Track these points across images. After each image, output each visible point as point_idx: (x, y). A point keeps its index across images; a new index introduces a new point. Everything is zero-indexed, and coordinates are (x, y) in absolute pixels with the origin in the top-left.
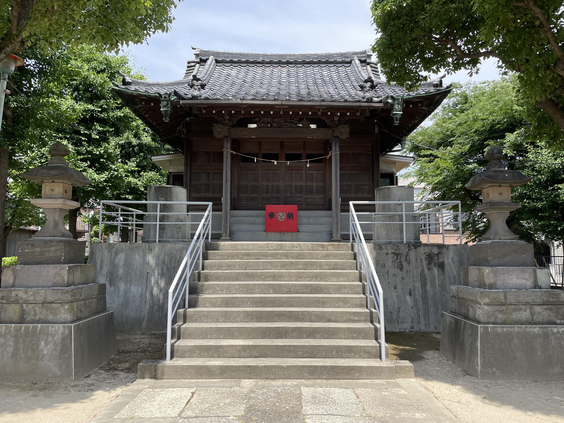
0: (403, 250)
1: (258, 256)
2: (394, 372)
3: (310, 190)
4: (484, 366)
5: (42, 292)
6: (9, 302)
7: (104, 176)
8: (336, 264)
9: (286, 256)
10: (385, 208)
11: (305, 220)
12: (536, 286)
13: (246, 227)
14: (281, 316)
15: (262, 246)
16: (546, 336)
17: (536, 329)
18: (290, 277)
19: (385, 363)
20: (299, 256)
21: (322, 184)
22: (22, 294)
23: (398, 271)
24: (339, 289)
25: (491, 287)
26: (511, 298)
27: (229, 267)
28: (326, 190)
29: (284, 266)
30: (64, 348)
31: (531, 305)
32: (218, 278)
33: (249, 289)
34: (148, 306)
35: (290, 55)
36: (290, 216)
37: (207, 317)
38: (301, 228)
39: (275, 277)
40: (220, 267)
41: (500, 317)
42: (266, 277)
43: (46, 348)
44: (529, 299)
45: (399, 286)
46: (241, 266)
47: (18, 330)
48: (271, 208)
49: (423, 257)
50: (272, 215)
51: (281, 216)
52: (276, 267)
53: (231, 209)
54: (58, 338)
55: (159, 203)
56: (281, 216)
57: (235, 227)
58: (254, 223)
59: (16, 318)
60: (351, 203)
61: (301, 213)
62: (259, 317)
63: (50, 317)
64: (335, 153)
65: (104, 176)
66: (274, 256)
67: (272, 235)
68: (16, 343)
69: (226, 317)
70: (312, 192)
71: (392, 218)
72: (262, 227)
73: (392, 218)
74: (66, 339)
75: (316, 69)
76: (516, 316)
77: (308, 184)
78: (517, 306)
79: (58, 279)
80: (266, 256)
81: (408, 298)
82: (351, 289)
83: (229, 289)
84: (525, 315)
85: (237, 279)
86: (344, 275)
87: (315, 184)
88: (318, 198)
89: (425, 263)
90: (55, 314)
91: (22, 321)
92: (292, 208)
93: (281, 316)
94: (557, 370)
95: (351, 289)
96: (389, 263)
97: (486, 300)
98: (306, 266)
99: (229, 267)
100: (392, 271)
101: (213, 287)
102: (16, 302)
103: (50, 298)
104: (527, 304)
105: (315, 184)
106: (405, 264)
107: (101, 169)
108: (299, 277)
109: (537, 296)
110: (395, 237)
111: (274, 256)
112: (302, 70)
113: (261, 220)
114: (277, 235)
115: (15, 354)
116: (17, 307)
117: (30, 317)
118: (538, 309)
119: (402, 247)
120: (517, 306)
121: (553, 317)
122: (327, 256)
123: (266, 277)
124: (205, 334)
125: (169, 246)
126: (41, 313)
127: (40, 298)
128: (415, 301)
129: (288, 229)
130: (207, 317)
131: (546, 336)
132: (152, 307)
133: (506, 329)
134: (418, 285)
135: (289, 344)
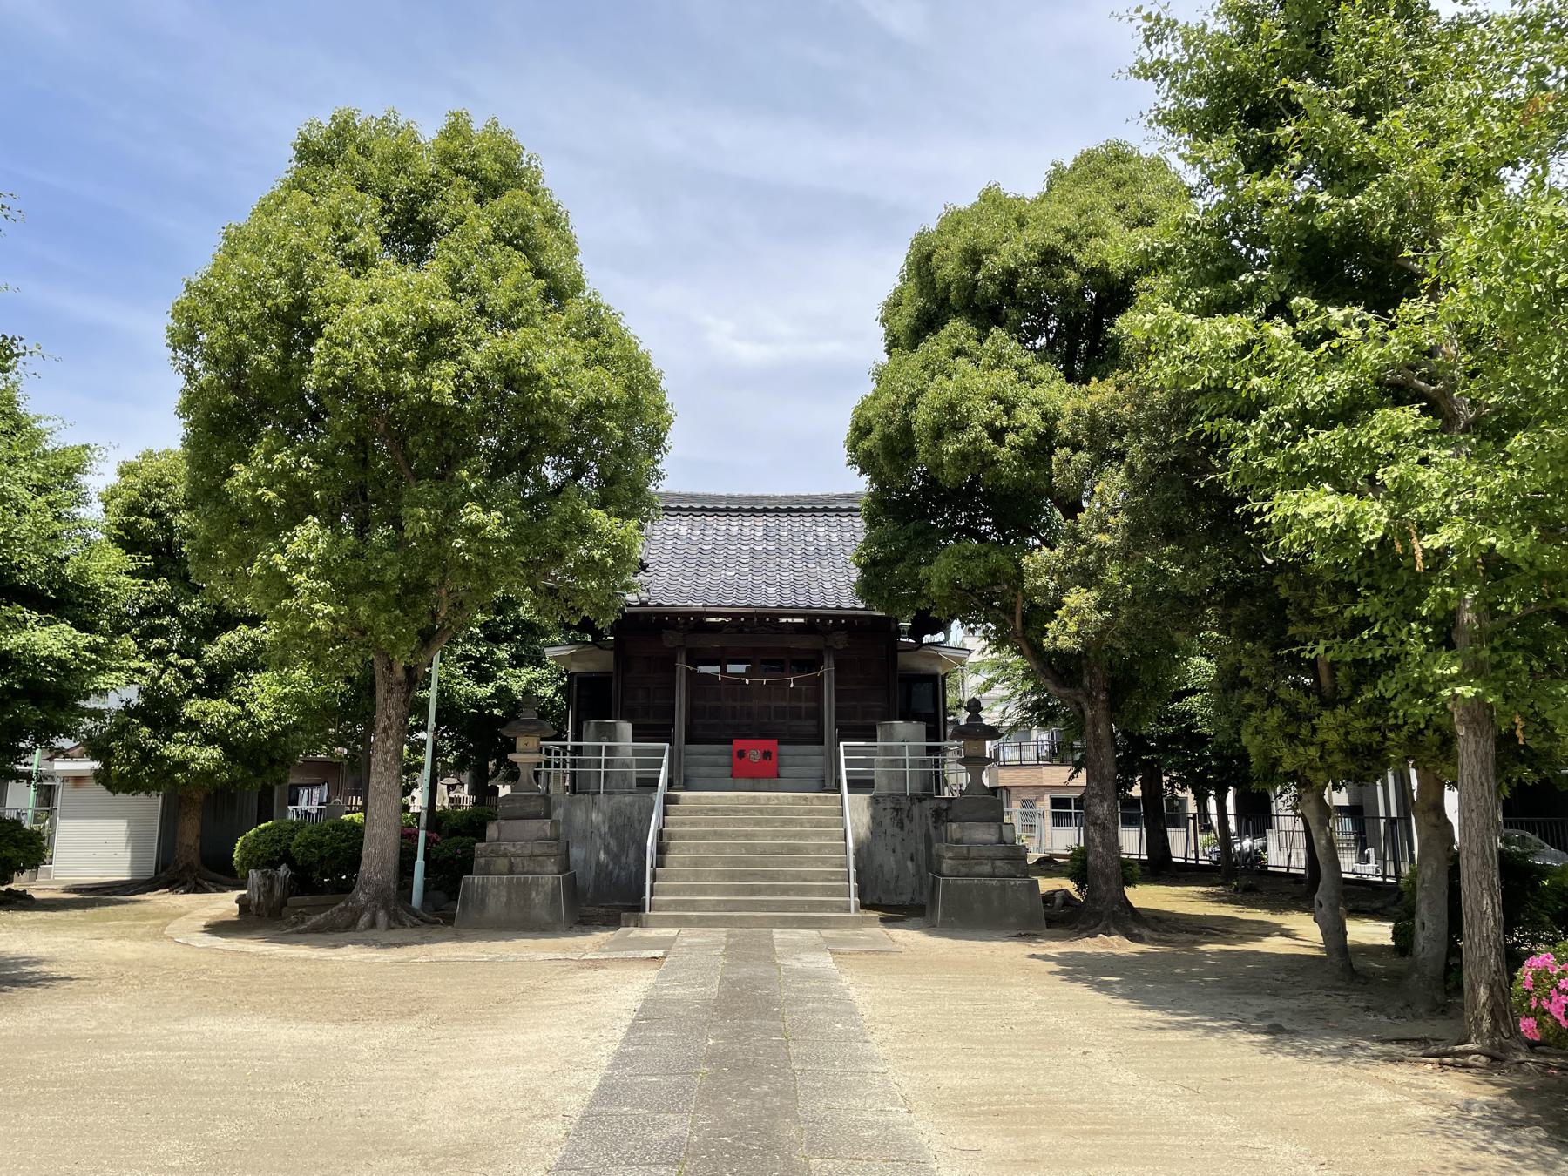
0: (906, 804)
1: (726, 811)
2: (862, 922)
3: (796, 714)
4: (945, 914)
5: (529, 845)
6: (498, 856)
7: (490, 689)
8: (819, 821)
9: (761, 812)
10: (887, 751)
11: (788, 760)
12: (1001, 841)
13: (704, 770)
14: (754, 875)
15: (731, 799)
16: (1003, 888)
17: (994, 882)
18: (764, 835)
19: (852, 914)
20: (775, 812)
21: (813, 704)
22: (510, 848)
23: (897, 830)
24: (820, 849)
25: (958, 842)
26: (974, 853)
27: (693, 824)
28: (817, 714)
29: (758, 823)
30: (554, 899)
31: (993, 859)
32: (682, 837)
33: (719, 849)
34: (593, 873)
35: (768, 498)
36: (767, 755)
37: (677, 876)
38: (784, 772)
39: (747, 836)
40: (683, 824)
41: (964, 870)
42: (737, 836)
43: (537, 898)
44: (991, 854)
45: (898, 850)
46: (707, 824)
47: (510, 881)
48: (739, 744)
49: (929, 813)
50: (741, 754)
51: (755, 755)
52: (748, 825)
53: (687, 742)
54: (548, 888)
55: (604, 744)
56: (755, 755)
57: (692, 770)
58: (715, 765)
59: (506, 870)
60: (842, 744)
61: (785, 749)
62: (732, 876)
63: (538, 869)
64: (827, 669)
65: (490, 689)
66: (745, 811)
67: (741, 782)
68: (509, 893)
69: (697, 876)
70: (799, 717)
71: (894, 763)
72: (727, 771)
73: (894, 763)
74: (555, 889)
75: (808, 521)
76: (978, 869)
77: (794, 704)
78: (980, 859)
79: (541, 834)
80: (736, 811)
81: (909, 864)
82: (833, 849)
83: (696, 849)
84: (987, 868)
85: (704, 838)
86: (826, 834)
87: (803, 705)
88: (808, 726)
89: (930, 821)
90: (542, 866)
91: (511, 872)
92: (770, 744)
93: (754, 875)
94: (1012, 920)
95: (833, 849)
96: (887, 821)
97: (950, 854)
98: (784, 823)
99: (693, 824)
100: (890, 831)
101: (680, 847)
102: (505, 855)
103: (537, 852)
104: (989, 858)
105: (803, 705)
106: (906, 822)
107: (482, 679)
108: (774, 836)
109: (1000, 850)
110: (896, 788)
111: (745, 811)
112: (786, 522)
113: (724, 759)
114: (749, 782)
115: (509, 903)
116: (506, 861)
117: (520, 869)
118: (998, 863)
119: (903, 800)
120: (980, 859)
121: (1013, 872)
122: (810, 812)
123: (737, 836)
124: (677, 891)
125: (618, 798)
126: (529, 866)
127: (527, 851)
128: (918, 866)
129: (765, 775)
130: (677, 876)
131: (1003, 888)
132: (598, 875)
133: (966, 881)
134: (922, 847)
135: (761, 896)
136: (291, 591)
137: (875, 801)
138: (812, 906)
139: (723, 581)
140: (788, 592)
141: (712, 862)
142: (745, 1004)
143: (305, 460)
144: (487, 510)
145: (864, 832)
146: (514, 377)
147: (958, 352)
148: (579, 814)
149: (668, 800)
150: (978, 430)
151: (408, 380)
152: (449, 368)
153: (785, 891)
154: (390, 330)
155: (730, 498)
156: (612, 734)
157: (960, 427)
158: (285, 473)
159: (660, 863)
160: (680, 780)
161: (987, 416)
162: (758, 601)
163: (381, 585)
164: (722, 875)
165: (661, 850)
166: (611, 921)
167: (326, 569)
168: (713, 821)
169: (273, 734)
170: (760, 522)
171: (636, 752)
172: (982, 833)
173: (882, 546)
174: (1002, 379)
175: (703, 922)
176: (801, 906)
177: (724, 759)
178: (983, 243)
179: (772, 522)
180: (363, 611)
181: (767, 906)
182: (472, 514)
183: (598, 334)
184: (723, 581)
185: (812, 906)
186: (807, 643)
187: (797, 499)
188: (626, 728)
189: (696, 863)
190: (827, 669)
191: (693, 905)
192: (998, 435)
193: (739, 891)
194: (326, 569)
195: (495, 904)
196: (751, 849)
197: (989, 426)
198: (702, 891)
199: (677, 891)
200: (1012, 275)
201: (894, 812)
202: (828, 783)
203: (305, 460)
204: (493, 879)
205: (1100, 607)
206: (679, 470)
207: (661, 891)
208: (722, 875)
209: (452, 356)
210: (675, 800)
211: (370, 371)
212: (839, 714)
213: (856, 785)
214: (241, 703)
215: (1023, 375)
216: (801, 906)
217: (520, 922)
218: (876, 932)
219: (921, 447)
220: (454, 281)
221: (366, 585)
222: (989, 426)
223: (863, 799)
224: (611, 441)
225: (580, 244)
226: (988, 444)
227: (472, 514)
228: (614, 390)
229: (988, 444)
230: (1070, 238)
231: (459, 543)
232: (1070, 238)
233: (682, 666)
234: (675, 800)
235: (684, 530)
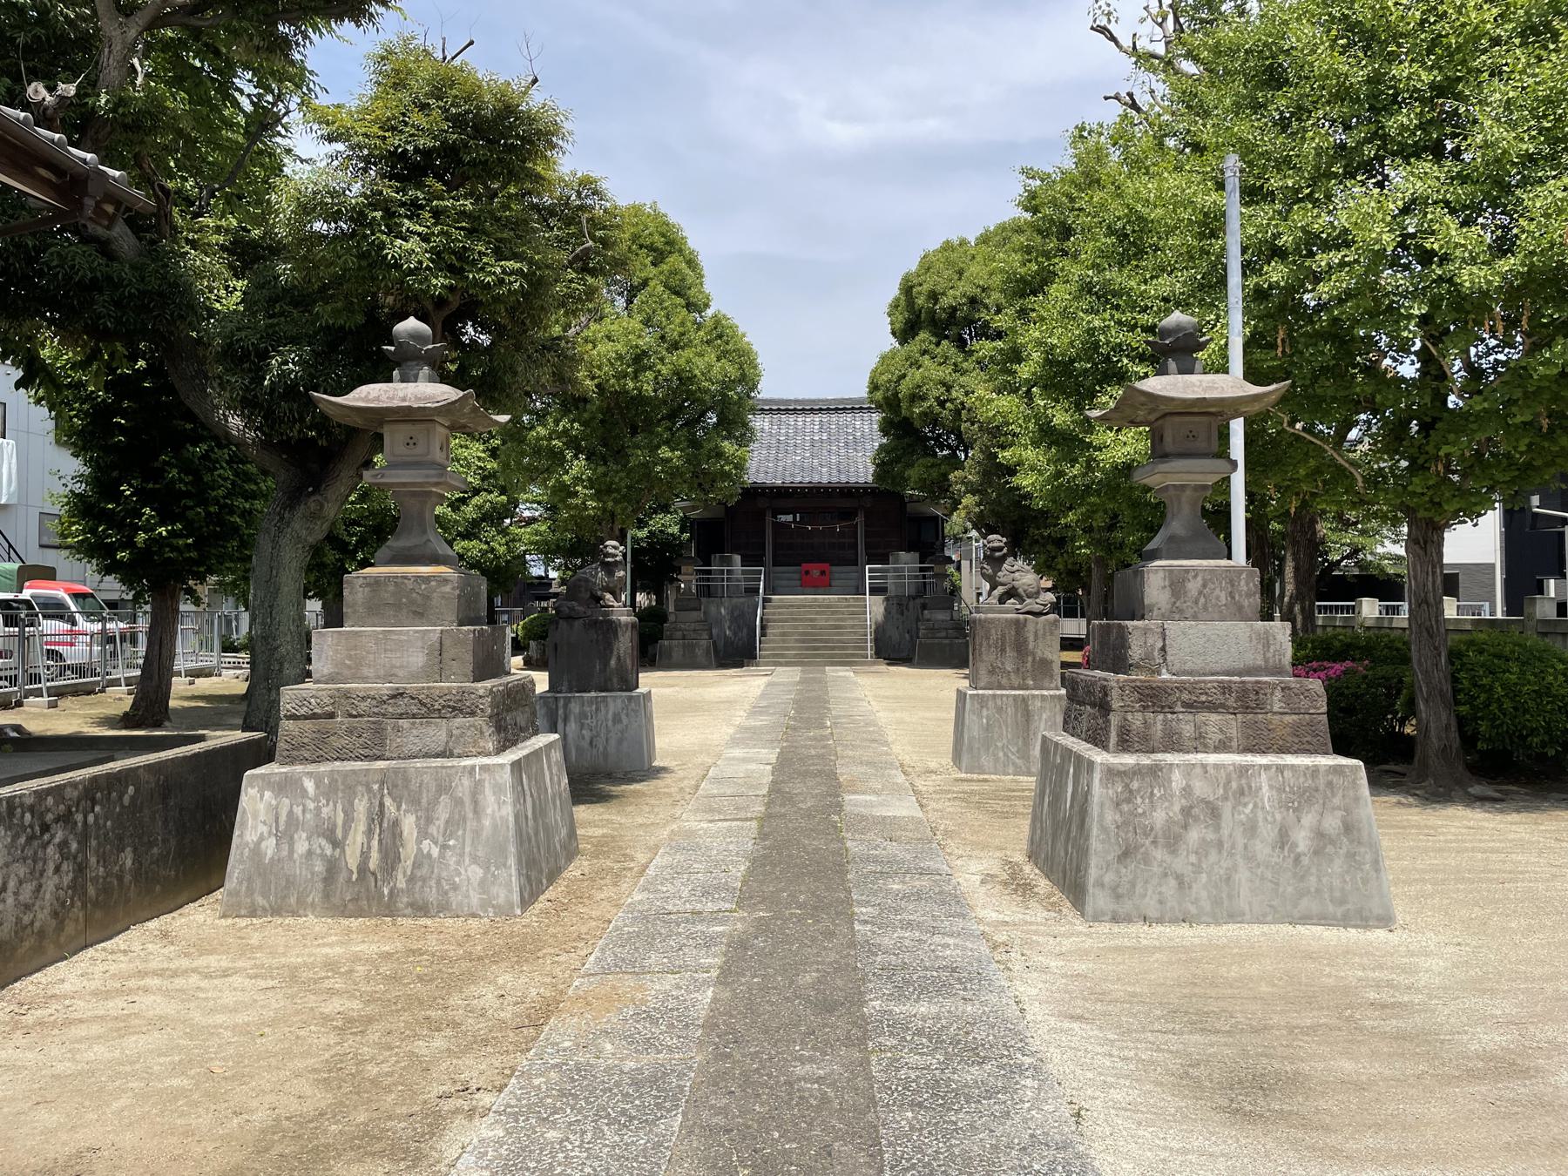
1: (799, 607)
2: (874, 664)
10: (895, 570)
17: (947, 641)
24: (853, 627)
29: (817, 613)
30: (708, 652)
33: (796, 627)
36: (823, 573)
43: (699, 652)
48: (806, 566)
50: (807, 573)
51: (816, 573)
61: (834, 568)
64: (860, 520)
67: (808, 590)
73: (899, 577)
92: (825, 566)
98: (833, 613)
112: (834, 418)
120: (939, 630)
124: (773, 649)
135: (821, 650)
136: (576, 494)
137: (887, 599)
138: (847, 656)
139: (794, 464)
140: (835, 472)
141: (792, 634)
142: (810, 710)
143: (576, 425)
144: (672, 450)
145: (880, 618)
146: (684, 378)
147: (925, 352)
148: (713, 609)
149: (765, 600)
150: (931, 402)
151: (631, 385)
152: (649, 375)
153: (833, 648)
154: (620, 357)
155: (796, 401)
156: (729, 562)
157: (923, 398)
158: (565, 431)
159: (763, 634)
160: (771, 589)
161: (936, 393)
162: (816, 479)
163: (618, 491)
164: (797, 641)
165: (763, 628)
166: (739, 664)
167: (591, 483)
168: (790, 609)
169: (507, 562)
170: (817, 418)
171: (744, 572)
172: (941, 616)
173: (888, 453)
174: (944, 372)
175: (787, 664)
176: (841, 656)
177: (796, 576)
178: (939, 289)
179: (825, 418)
180: (610, 504)
181: (822, 656)
182: (665, 452)
183: (721, 336)
184: (794, 464)
185: (847, 656)
186: (846, 504)
187: (842, 401)
188: (737, 558)
189: (783, 634)
190: (860, 520)
191: (782, 656)
192: (942, 404)
193: (807, 649)
194: (591, 483)
195: (677, 655)
196: (813, 627)
197: (937, 399)
198: (788, 649)
199: (773, 649)
200: (954, 309)
201: (897, 606)
202: (859, 591)
203: (576, 425)
204: (675, 642)
205: (978, 504)
206: (768, 389)
207: (763, 648)
208: (797, 641)
209: (650, 368)
210: (770, 600)
211: (612, 381)
212: (868, 546)
213: (874, 591)
214: (487, 543)
215: (957, 369)
216: (841, 656)
217: (690, 663)
218: (883, 668)
219: (904, 405)
220: (647, 322)
221: (609, 491)
222: (937, 399)
223: (879, 599)
224: (732, 407)
225: (704, 260)
226: (937, 409)
227: (665, 452)
228: (733, 371)
229: (937, 409)
230: (984, 290)
231: (658, 468)
232: (984, 290)
233: (769, 519)
234: (770, 600)
235: (766, 425)
